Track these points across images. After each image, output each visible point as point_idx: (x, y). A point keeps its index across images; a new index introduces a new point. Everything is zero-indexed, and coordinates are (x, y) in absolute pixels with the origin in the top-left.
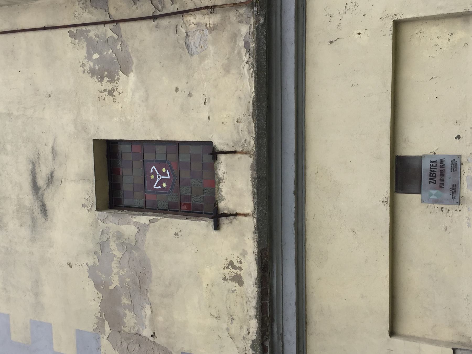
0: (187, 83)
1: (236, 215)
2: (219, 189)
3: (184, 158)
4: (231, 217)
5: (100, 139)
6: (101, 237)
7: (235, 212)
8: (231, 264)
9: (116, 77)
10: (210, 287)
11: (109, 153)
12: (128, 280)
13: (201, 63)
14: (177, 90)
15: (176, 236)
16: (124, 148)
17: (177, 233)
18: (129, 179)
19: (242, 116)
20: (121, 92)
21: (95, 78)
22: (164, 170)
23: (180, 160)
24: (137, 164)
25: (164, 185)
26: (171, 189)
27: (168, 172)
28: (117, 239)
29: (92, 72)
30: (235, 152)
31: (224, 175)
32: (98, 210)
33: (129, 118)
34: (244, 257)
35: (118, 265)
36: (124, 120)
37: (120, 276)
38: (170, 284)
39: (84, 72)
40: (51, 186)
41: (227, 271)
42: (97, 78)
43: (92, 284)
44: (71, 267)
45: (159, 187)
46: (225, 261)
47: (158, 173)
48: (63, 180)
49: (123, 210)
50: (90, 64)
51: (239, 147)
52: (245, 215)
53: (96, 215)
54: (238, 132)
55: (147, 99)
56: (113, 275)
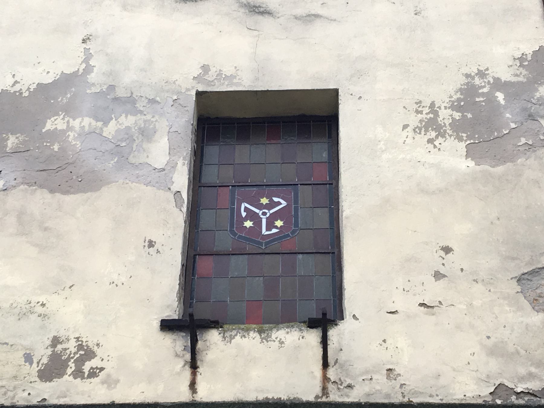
0: (462, 270)
1: (194, 366)
2: (248, 330)
3: (305, 265)
4: (188, 356)
5: (340, 102)
6: (143, 99)
7: (199, 363)
8: (89, 354)
9: (464, 135)
10: (39, 309)
11: (307, 121)
12: (56, 147)
13: (504, 298)
14: (447, 250)
15: (147, 244)
16: (318, 151)
17: (153, 246)
18: (259, 156)
19: (401, 380)
20: (436, 143)
21: (459, 95)
22: (279, 223)
23: (300, 256)
24: (290, 173)
25: (248, 224)
26: (240, 237)
27: (274, 231)
28: (140, 129)
29: (469, 91)
30: (325, 365)
31: (277, 343)
32: (200, 94)
33: (385, 156)
34: (103, 383)
35: (87, 129)
36: (379, 147)
37: (64, 132)
38: (46, 229)
39: (467, 76)
40: (242, 10)
41: (72, 346)
42: (459, 100)
43: (48, 79)
44: (84, 41)
45: (244, 214)
46: (95, 341)
47: (272, 211)
48: (256, 33)
49: (197, 142)
50: (484, 87)
51: (337, 374)
52: (193, 386)
53: (188, 90)
54: (367, 372)
55: (424, 191)
56: (66, 119)
